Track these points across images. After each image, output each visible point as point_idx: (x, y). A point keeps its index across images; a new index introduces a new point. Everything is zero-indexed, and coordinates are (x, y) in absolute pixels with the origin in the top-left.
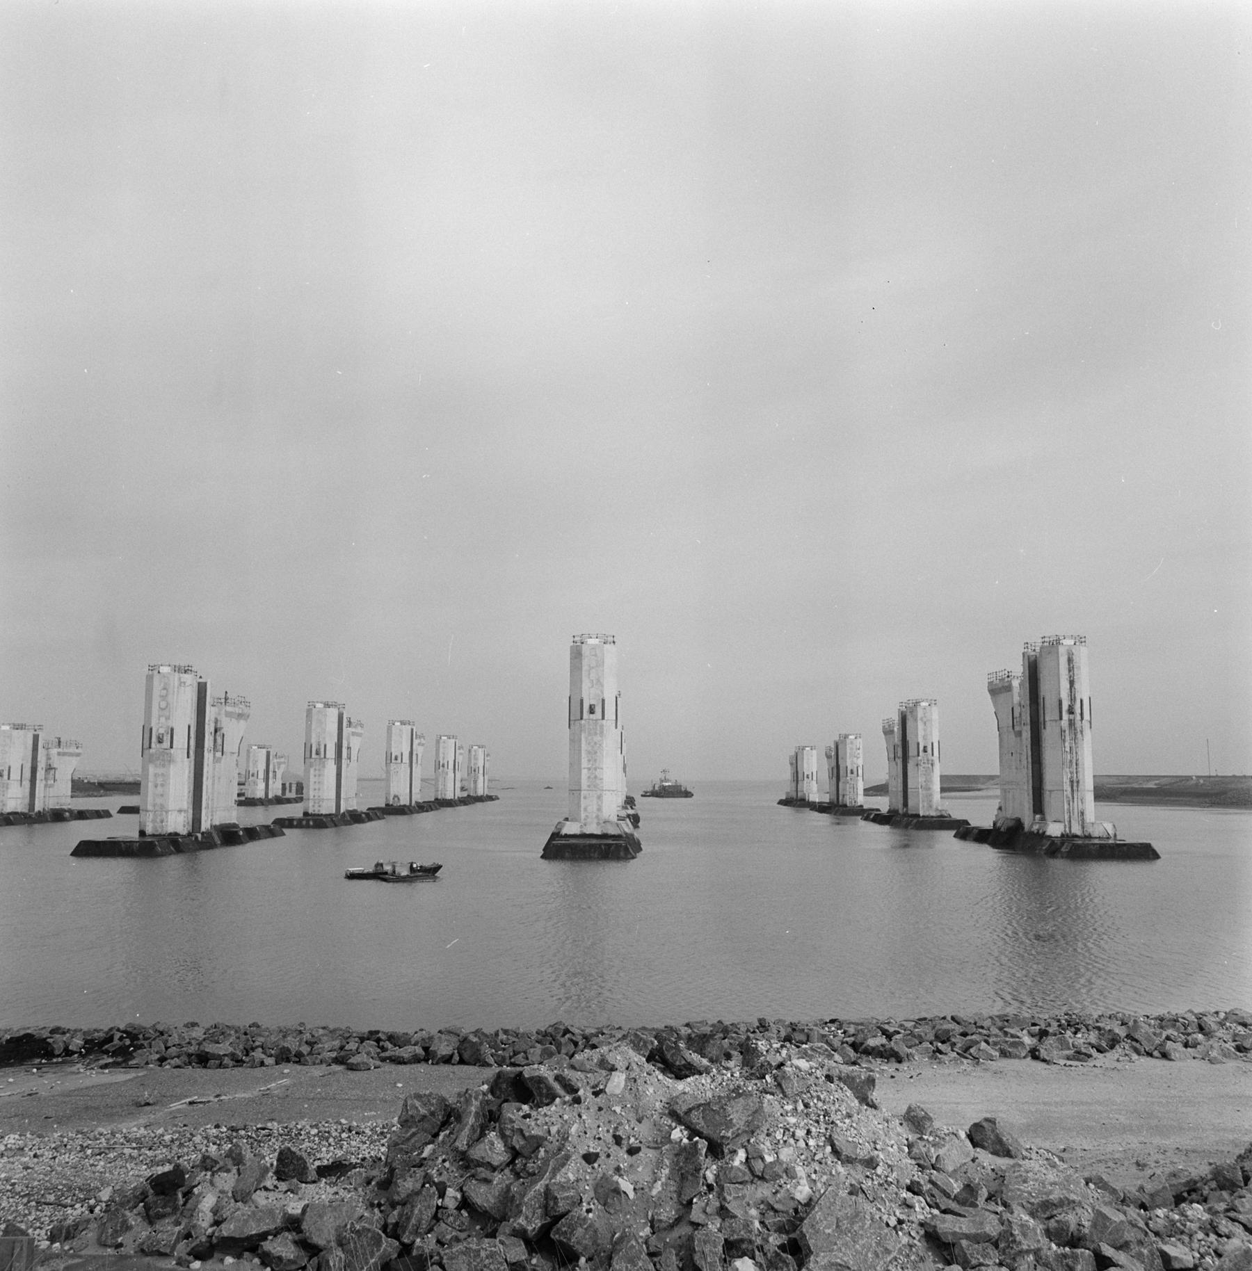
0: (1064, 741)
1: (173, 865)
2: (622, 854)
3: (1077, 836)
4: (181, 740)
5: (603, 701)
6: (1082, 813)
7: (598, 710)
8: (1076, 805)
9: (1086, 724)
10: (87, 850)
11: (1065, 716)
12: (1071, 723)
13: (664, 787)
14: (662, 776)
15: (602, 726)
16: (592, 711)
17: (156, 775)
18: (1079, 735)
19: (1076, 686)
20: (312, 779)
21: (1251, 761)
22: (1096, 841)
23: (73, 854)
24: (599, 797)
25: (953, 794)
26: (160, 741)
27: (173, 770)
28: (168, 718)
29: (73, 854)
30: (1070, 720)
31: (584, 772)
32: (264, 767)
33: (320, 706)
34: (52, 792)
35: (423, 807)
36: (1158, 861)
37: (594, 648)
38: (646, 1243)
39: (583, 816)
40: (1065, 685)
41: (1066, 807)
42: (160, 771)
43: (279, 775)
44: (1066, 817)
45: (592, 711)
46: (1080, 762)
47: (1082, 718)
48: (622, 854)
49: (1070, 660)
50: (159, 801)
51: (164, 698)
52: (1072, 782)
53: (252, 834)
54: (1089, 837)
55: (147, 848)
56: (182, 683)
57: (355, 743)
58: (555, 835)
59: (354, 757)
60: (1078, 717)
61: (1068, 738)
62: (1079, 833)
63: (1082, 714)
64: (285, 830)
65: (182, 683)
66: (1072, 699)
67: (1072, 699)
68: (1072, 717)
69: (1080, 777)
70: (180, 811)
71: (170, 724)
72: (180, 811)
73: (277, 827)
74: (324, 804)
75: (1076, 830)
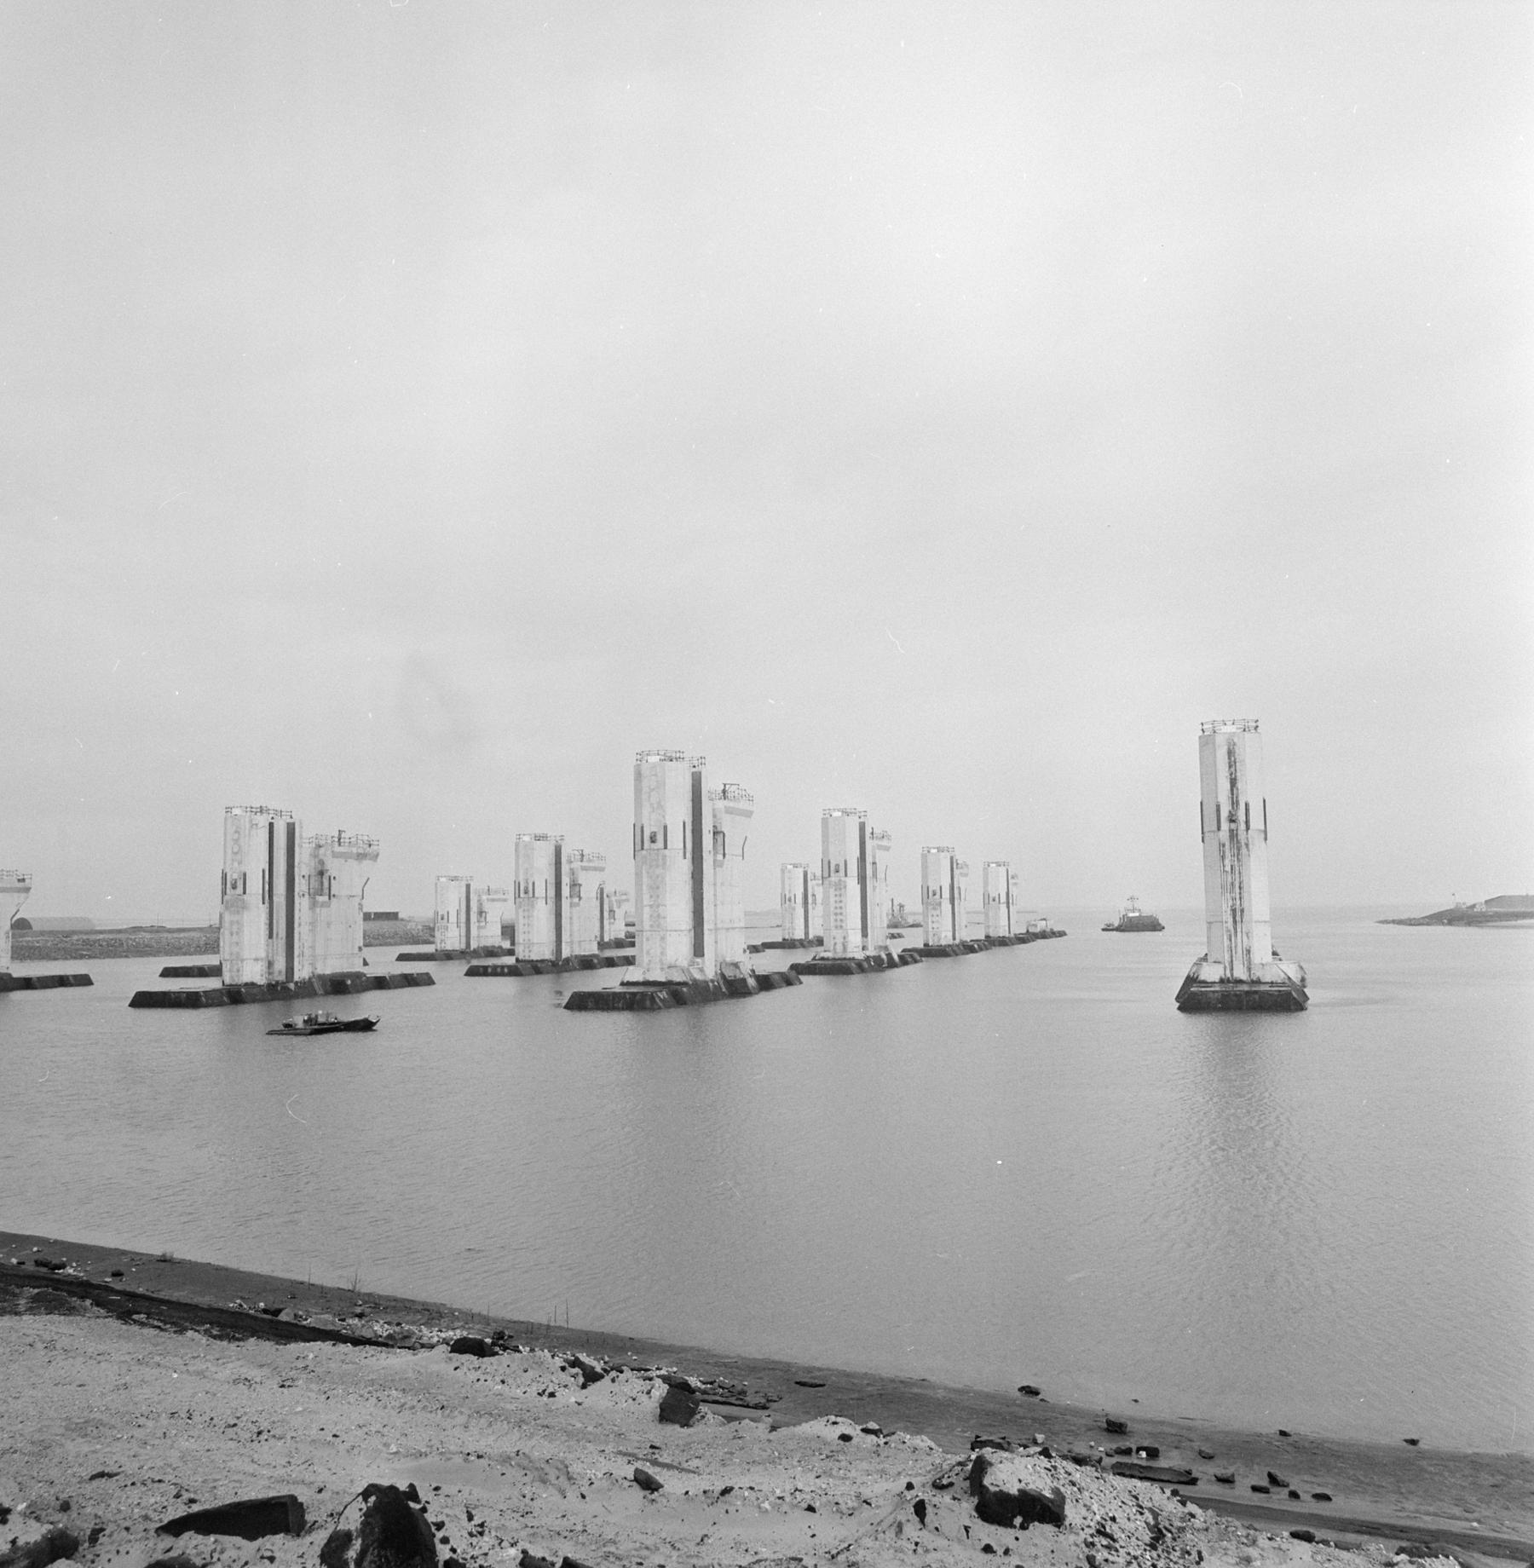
0: (1223, 858)
1: (673, 1021)
2: (648, 1003)
3: (1241, 982)
4: (255, 885)
5: (665, 828)
6: (1249, 951)
7: (660, 838)
8: (1241, 942)
9: (1254, 836)
10: (580, 1003)
11: (1225, 826)
12: (1233, 835)
13: (1130, 919)
14: (1129, 905)
15: (664, 857)
16: (653, 840)
17: (232, 923)
18: (1244, 850)
19: (1239, 785)
20: (521, 921)
21: (1532, 880)
22: (1267, 988)
23: (131, 1005)
24: (663, 939)
25: (1520, 922)
26: (234, 887)
27: (246, 916)
28: (240, 863)
29: (131, 1005)
30: (1231, 831)
31: (647, 910)
32: (802, 890)
33: (837, 814)
34: (484, 932)
35: (1022, 939)
36: (1303, 1014)
37: (654, 766)
38: (283, 1421)
39: (646, 960)
40: (1224, 785)
41: (1226, 943)
42: (236, 918)
43: (619, 913)
44: (1227, 957)
45: (653, 840)
46: (1245, 885)
47: (1248, 828)
48: (648, 1003)
49: (1230, 753)
50: (236, 949)
51: (236, 841)
52: (1234, 911)
53: (766, 983)
54: (1258, 982)
55: (636, 1000)
56: (254, 825)
57: (882, 859)
58: (1191, 980)
59: (880, 875)
60: (1243, 826)
61: (1228, 854)
62: (1244, 977)
63: (1247, 822)
64: (802, 978)
65: (254, 825)
66: (1235, 803)
67: (1235, 803)
68: (1233, 826)
69: (1246, 905)
70: (256, 960)
71: (243, 869)
72: (256, 960)
73: (793, 973)
74: (535, 948)
75: (1240, 973)
